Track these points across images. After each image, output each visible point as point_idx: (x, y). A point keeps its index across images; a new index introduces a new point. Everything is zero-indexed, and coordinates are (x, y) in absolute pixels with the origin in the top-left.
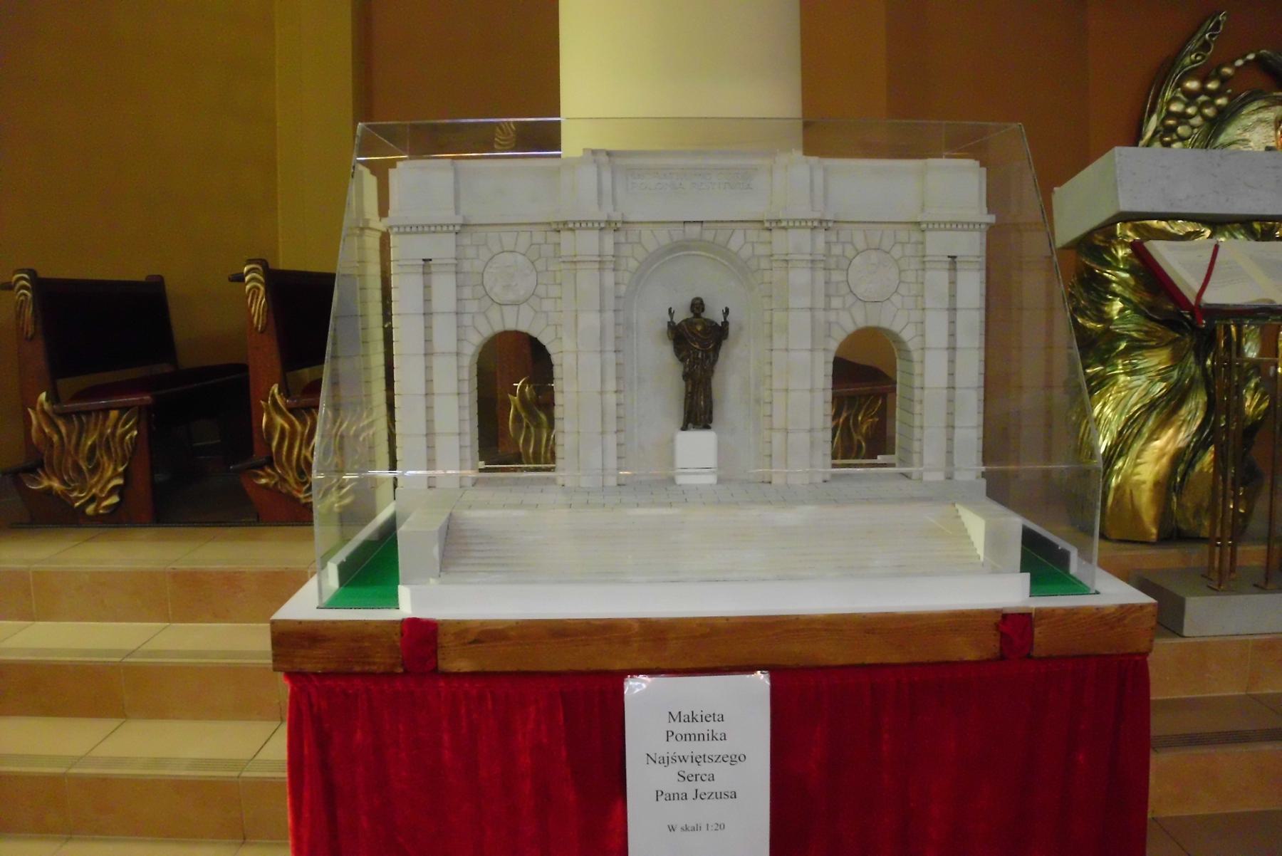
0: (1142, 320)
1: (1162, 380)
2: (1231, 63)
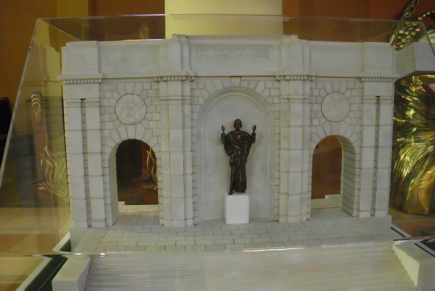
0: (424, 119)
1: (432, 145)
2: (421, 16)
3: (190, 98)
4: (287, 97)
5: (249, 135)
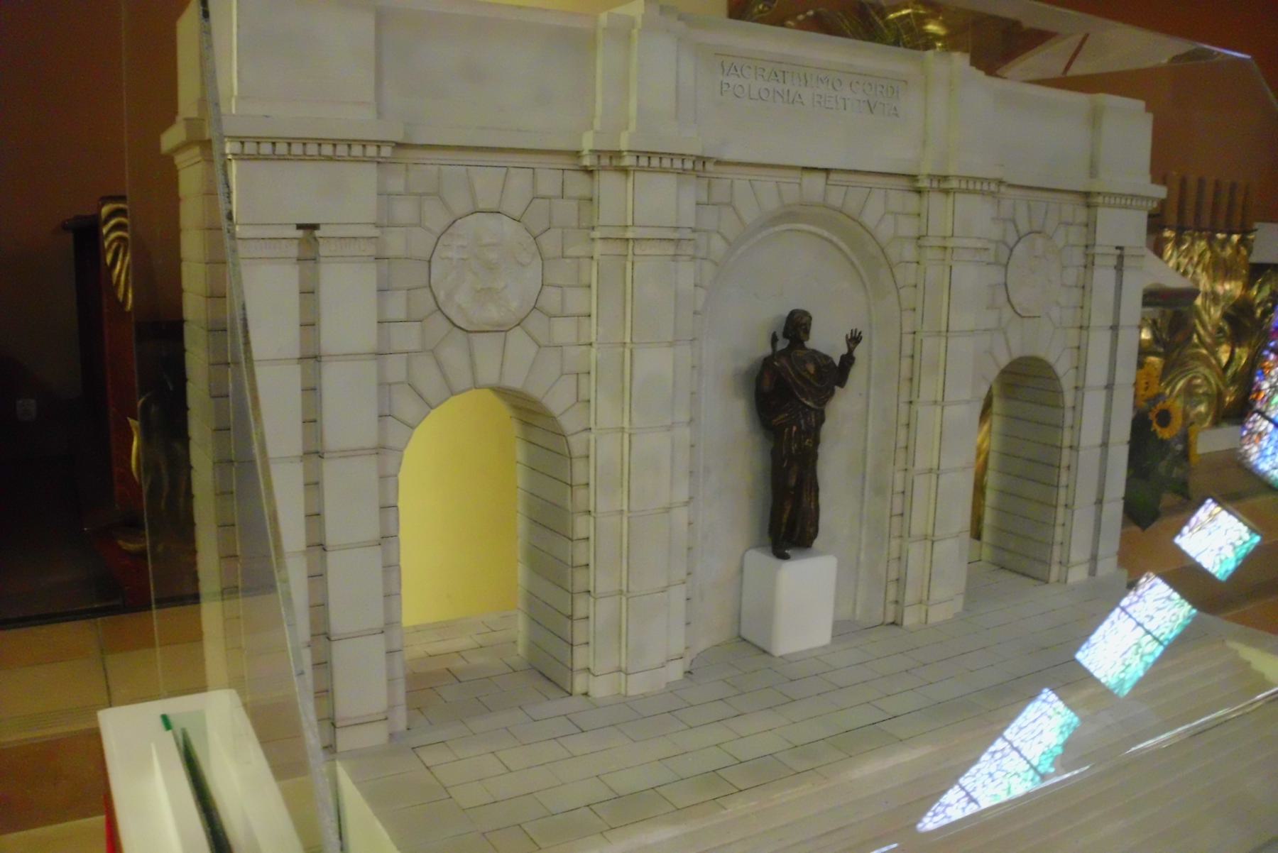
5: (833, 363)
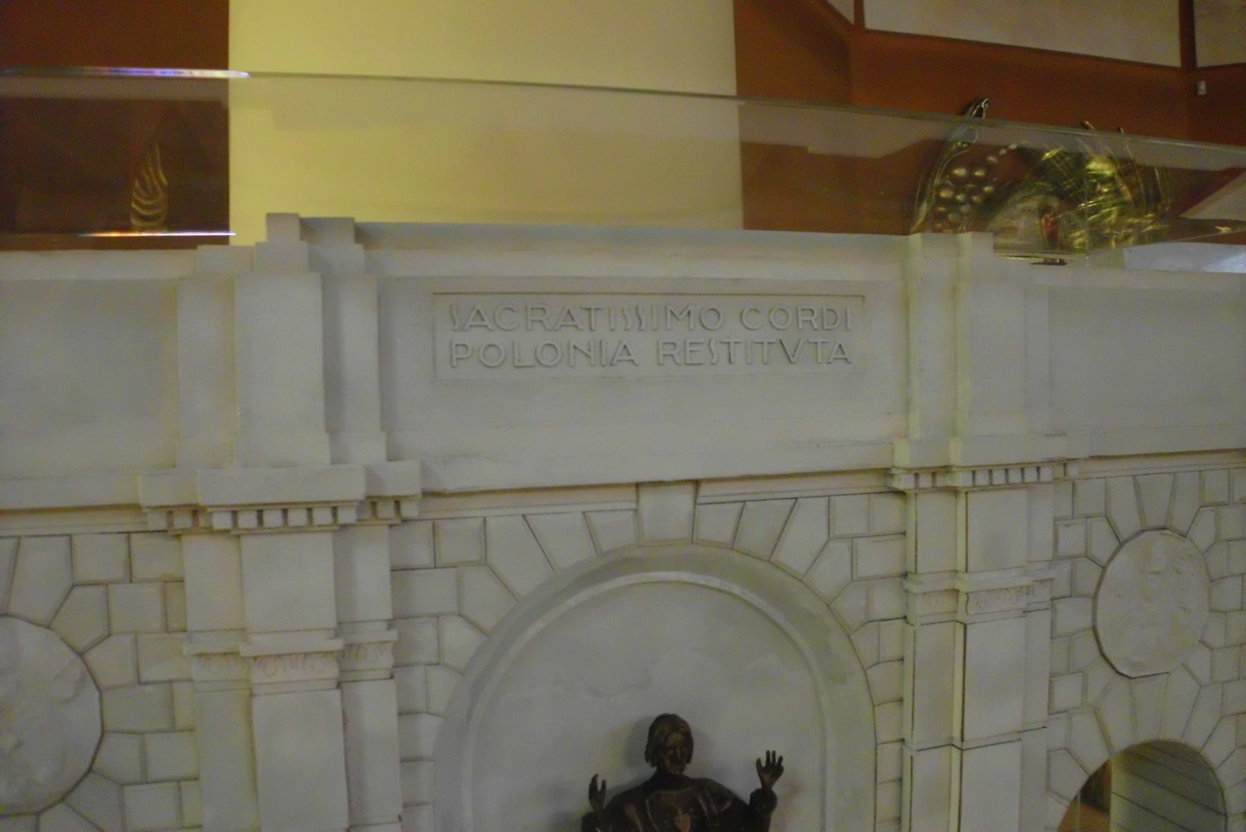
3: (393, 635)
4: (947, 584)
